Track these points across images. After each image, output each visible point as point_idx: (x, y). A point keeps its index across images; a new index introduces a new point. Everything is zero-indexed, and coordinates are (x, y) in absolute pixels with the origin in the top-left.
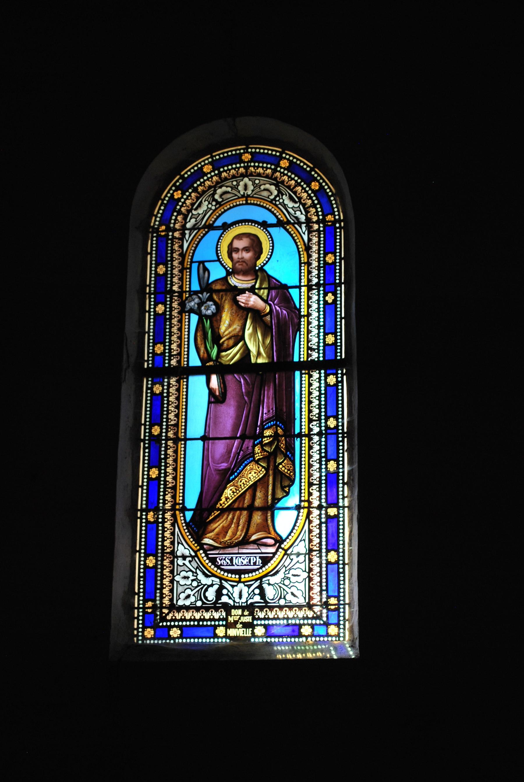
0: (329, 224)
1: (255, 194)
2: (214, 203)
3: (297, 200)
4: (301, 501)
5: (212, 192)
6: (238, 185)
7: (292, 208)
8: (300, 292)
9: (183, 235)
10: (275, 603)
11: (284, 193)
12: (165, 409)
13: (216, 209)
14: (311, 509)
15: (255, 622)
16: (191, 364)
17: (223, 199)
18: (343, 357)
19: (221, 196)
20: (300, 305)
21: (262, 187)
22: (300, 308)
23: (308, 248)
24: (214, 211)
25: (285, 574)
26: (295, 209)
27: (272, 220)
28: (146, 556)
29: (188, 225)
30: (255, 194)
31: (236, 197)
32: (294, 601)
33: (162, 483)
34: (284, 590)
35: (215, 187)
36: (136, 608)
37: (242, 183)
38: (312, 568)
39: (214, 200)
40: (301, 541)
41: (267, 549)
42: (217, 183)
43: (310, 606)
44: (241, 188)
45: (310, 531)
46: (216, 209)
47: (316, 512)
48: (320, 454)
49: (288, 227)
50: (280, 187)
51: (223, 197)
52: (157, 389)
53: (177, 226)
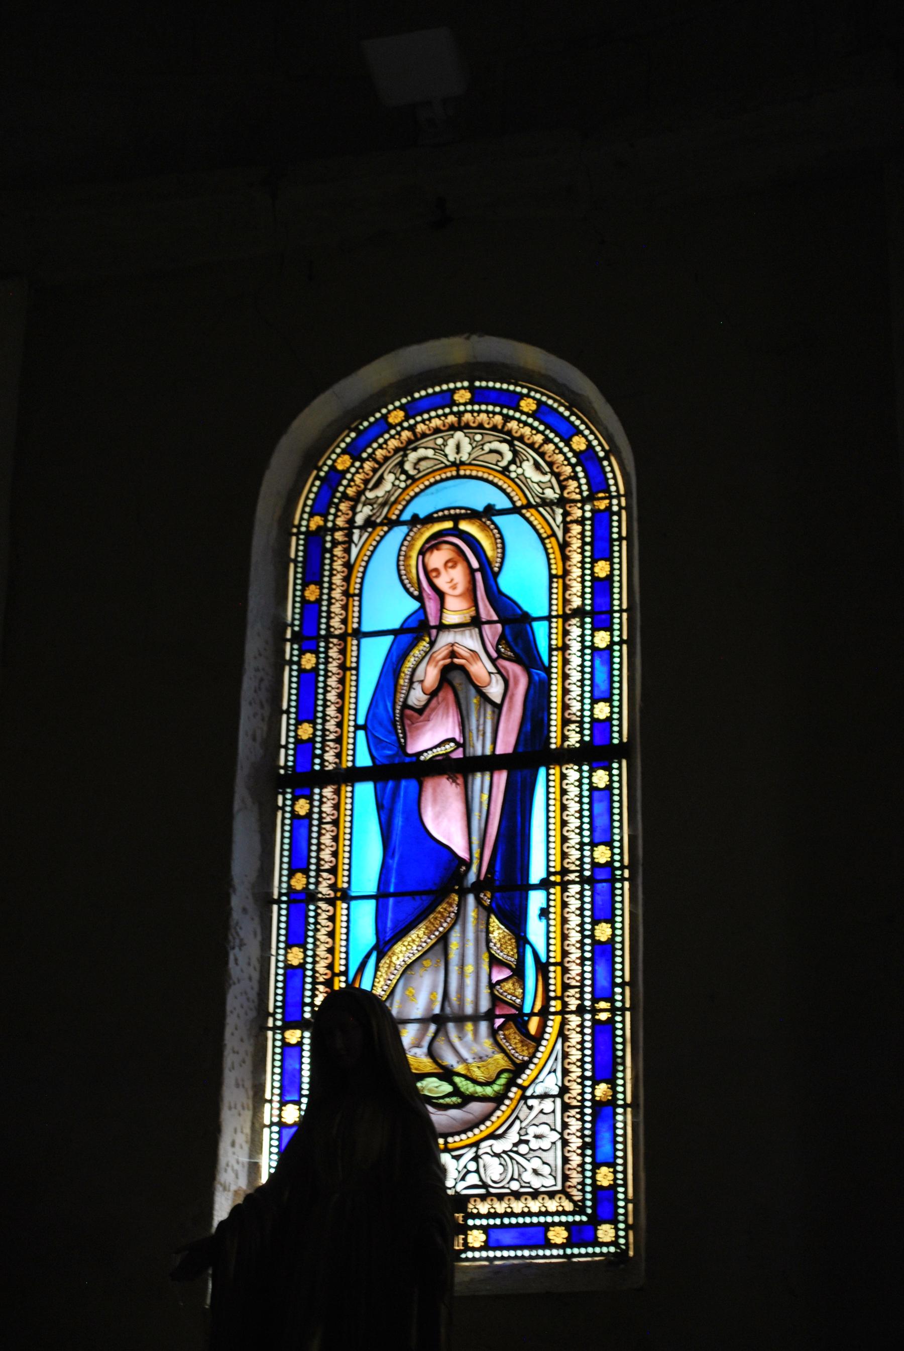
0: (601, 495)
1: (474, 459)
2: (403, 477)
3: (547, 469)
4: (549, 874)
5: (400, 459)
6: (445, 445)
7: (537, 483)
8: (550, 628)
9: (349, 535)
10: (503, 1187)
11: (525, 458)
12: (312, 920)
13: (407, 487)
14: (567, 1016)
15: (470, 1222)
16: (359, 764)
17: (418, 470)
18: (625, 740)
19: (415, 465)
20: (550, 661)
21: (487, 448)
22: (550, 667)
23: (564, 546)
24: (404, 489)
25: (520, 1135)
26: (543, 486)
27: (502, 502)
28: (299, 722)
29: (360, 520)
30: (474, 459)
31: (443, 465)
32: (536, 1183)
33: (324, 614)
34: (518, 1163)
35: (403, 450)
36: (270, 1029)
37: (452, 443)
38: (566, 805)
39: (404, 472)
40: (550, 1072)
41: (490, 836)
42: (410, 442)
43: (564, 1192)
44: (450, 450)
45: (565, 1055)
46: (407, 487)
47: (574, 1020)
48: (582, 931)
49: (528, 515)
50: (518, 448)
51: (418, 467)
52: (302, 807)
53: (340, 522)
